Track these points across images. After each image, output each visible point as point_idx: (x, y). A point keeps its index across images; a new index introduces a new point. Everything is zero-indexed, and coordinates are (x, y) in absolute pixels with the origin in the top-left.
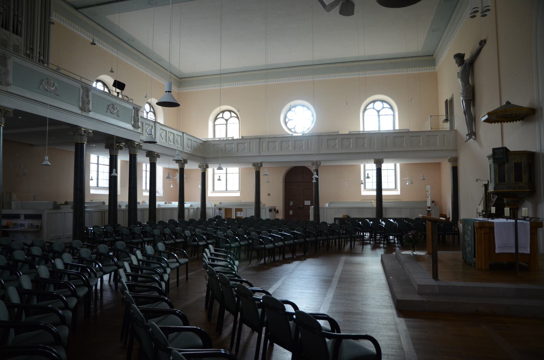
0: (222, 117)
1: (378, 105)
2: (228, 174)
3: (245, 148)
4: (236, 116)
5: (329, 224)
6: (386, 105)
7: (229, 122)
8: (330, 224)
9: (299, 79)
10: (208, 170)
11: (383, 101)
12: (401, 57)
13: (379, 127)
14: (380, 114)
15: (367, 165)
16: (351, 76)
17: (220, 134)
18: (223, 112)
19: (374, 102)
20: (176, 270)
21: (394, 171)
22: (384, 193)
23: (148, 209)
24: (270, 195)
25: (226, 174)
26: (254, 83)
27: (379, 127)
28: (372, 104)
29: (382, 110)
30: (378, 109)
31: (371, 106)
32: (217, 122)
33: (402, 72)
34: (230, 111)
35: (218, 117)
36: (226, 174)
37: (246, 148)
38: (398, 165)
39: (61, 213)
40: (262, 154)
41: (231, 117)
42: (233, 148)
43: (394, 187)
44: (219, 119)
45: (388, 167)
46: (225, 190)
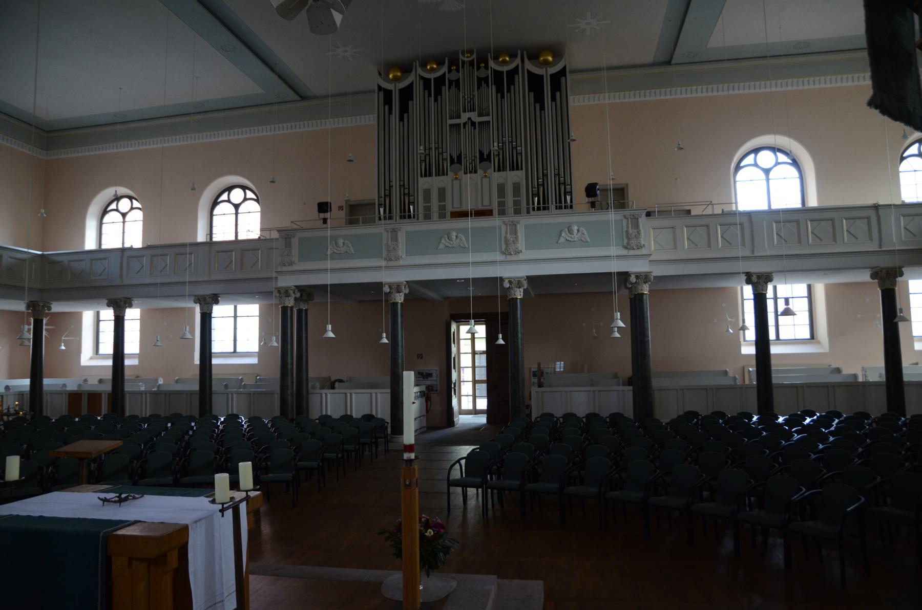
0: (227, 199)
1: (766, 158)
2: (233, 315)
3: (143, 266)
4: (255, 198)
5: (316, 419)
6: (782, 157)
7: (128, 218)
8: (585, 416)
9: (214, 135)
10: (110, 309)
11: (774, 149)
12: (853, 47)
13: (123, 243)
14: (240, 211)
15: (240, 307)
16: (270, 133)
17: (111, 241)
18: (229, 189)
19: (756, 151)
20: (232, 512)
21: (806, 300)
22: (774, 350)
23: (885, 384)
24: (422, 358)
25: (235, 317)
26: (308, 126)
27: (123, 243)
28: (752, 156)
29: (775, 168)
30: (124, 211)
31: (750, 159)
32: (107, 218)
33: (825, 83)
34: (244, 188)
35: (742, 164)
36: (235, 317)
37: (168, 266)
38: (820, 290)
39: (561, 391)
40: (756, 254)
41: (132, 208)
42: (105, 269)
43: (808, 336)
44: (221, 205)
45: (133, 315)
46: (232, 351)
